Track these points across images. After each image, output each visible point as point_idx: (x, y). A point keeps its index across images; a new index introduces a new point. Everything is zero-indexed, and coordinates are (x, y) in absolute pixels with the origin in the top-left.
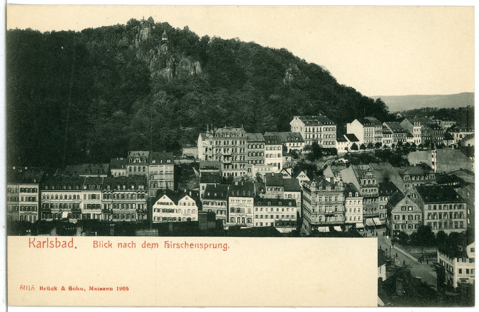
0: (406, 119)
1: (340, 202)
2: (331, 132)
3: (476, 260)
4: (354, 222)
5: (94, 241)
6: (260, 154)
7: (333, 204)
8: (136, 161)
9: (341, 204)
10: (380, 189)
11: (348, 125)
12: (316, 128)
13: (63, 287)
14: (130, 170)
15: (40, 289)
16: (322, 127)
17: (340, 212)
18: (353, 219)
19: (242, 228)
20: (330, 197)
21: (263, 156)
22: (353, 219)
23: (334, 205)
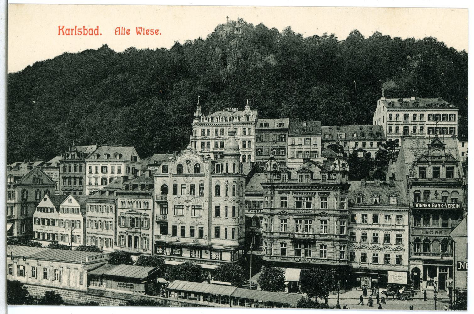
0: (71, 197)
2: (446, 123)
3: (380, 312)
4: (384, 268)
6: (279, 151)
7: (315, 215)
8: (72, 155)
11: (365, 38)
12: (411, 115)
14: (65, 171)
16: (426, 114)
17: (334, 238)
19: (230, 284)
21: (285, 155)
22: (369, 259)
23: (316, 218)
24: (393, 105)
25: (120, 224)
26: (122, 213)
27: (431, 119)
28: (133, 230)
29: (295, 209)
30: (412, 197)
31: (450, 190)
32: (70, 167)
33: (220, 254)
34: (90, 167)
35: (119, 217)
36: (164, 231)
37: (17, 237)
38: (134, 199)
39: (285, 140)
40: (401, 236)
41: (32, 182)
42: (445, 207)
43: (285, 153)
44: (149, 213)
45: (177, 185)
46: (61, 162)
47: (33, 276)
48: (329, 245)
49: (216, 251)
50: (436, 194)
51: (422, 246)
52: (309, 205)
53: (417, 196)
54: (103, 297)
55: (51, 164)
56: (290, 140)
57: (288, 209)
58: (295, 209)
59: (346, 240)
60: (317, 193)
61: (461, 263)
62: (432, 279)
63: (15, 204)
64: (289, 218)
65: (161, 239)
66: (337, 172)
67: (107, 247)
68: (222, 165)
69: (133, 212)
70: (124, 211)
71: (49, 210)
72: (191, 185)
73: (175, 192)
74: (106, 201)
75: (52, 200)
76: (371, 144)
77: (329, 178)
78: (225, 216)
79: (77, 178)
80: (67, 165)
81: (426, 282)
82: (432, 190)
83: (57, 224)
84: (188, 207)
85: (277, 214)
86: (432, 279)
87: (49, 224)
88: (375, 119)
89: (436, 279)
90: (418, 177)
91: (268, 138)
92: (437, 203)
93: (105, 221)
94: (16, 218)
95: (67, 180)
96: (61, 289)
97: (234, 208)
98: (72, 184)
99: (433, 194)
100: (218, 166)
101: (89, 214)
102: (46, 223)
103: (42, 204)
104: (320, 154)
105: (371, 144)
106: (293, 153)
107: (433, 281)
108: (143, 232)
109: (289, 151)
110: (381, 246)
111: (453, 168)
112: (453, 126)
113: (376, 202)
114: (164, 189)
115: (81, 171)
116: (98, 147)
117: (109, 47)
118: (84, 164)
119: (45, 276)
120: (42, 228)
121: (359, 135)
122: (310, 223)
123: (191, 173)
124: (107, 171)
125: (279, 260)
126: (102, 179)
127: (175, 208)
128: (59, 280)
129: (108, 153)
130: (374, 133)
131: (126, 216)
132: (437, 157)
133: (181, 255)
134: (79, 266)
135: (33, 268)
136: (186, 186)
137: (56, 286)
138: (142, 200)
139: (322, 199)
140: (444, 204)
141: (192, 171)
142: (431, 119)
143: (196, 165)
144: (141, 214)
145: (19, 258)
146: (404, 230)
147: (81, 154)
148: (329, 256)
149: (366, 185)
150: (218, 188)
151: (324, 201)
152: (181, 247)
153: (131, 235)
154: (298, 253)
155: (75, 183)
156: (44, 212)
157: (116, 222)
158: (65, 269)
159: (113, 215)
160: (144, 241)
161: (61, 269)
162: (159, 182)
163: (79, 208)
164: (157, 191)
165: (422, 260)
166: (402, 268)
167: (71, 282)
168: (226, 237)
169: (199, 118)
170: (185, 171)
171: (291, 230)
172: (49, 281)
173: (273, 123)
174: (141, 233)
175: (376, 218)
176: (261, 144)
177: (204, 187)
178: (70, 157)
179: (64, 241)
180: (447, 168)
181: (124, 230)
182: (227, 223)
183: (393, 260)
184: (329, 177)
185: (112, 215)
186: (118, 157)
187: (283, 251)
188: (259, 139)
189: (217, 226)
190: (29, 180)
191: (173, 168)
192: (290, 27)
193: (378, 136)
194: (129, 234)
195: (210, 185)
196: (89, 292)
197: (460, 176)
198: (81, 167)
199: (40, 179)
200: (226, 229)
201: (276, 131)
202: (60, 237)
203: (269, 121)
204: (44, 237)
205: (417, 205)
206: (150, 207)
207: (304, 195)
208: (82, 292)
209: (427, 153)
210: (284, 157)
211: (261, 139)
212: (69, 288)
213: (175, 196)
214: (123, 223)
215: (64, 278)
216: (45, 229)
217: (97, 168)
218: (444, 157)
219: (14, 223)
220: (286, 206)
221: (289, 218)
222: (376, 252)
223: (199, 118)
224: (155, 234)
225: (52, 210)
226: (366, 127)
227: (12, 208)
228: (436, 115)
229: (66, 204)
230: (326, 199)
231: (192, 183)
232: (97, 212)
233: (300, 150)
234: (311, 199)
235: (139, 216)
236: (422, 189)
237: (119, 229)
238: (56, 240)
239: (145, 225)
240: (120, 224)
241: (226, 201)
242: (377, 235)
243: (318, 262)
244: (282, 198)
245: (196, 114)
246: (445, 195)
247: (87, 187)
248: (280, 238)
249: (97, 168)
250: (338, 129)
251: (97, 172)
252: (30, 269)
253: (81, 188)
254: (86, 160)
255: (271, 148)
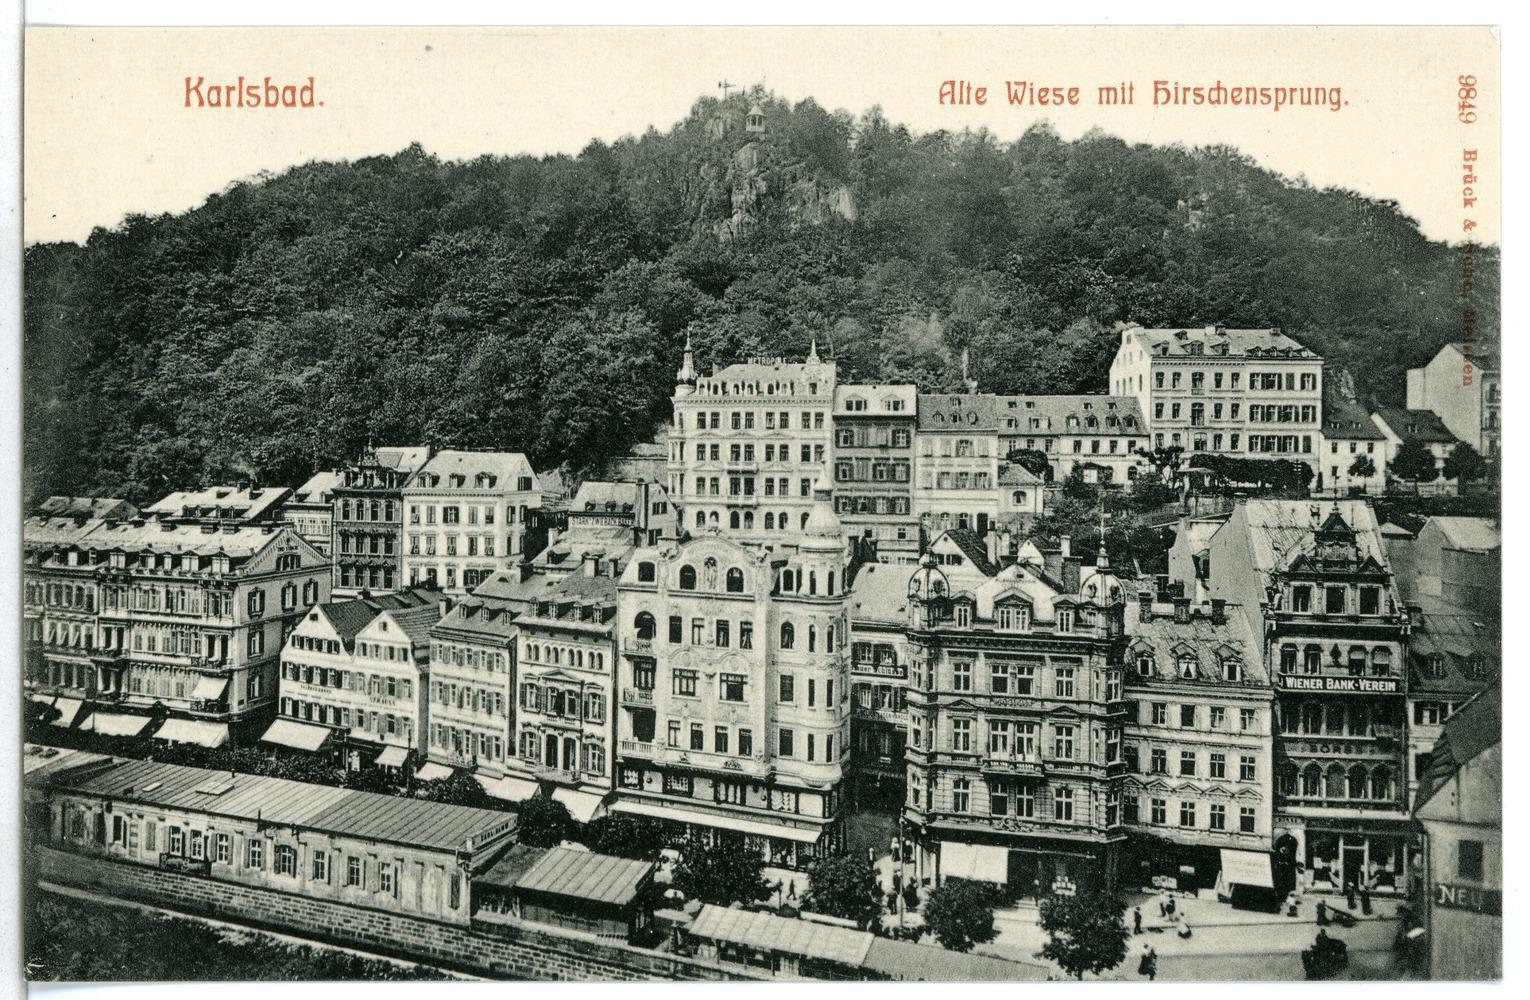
0: (385, 616)
1: (1084, 708)
5: (1156, 83)
7: (1042, 714)
8: (365, 476)
9: (1092, 717)
10: (930, 851)
13: (1473, 224)
14: (346, 515)
15: (1466, 153)
18: (1203, 819)
19: (854, 923)
20: (1021, 671)
22: (1203, 819)
24: (1165, 350)
25: (523, 702)
26: (529, 676)
27: (1258, 384)
28: (560, 722)
29: (991, 698)
30: (1277, 660)
31: (1370, 645)
32: (360, 506)
33: (793, 796)
34: (413, 510)
35: (522, 685)
36: (644, 722)
37: (239, 716)
38: (564, 644)
39: (908, 442)
40: (1252, 760)
41: (274, 567)
42: (1358, 688)
43: (908, 475)
44: (606, 683)
45: (679, 619)
46: (337, 494)
47: (318, 874)
48: (1080, 792)
49: (784, 789)
50: (1336, 653)
51: (1301, 781)
52: (1025, 686)
53: (1288, 658)
54: (515, 944)
55: (306, 496)
56: (919, 443)
57: (975, 696)
58: (991, 698)
59: (1119, 776)
60: (1048, 660)
61: (1444, 889)
62: (1326, 865)
63: (233, 629)
64: (975, 720)
65: (638, 752)
66: (1099, 609)
67: (489, 758)
68: (799, 573)
69: (559, 677)
70: (537, 671)
71: (325, 646)
72: (718, 622)
73: (675, 635)
74: (489, 640)
75: (331, 620)
76: (1113, 445)
77: (1078, 622)
78: (807, 702)
79: (380, 535)
80: (353, 502)
81: (1311, 872)
82: (1327, 643)
83: (345, 682)
84: (711, 677)
85: (947, 707)
86: (1326, 865)
87: (324, 682)
88: (1116, 373)
89: (1338, 865)
90: (1291, 611)
91: (865, 438)
92: (1340, 679)
93: (483, 692)
94: (236, 666)
95: (353, 541)
96: (399, 915)
97: (830, 683)
98: (367, 550)
99: (1327, 653)
100: (788, 574)
101: (436, 667)
102: (317, 679)
103: (305, 628)
104: (995, 481)
105: (1113, 445)
106: (930, 475)
107: (1329, 869)
108: (588, 729)
109: (919, 467)
110: (1205, 786)
111: (1376, 591)
112: (1312, 403)
113: (1188, 673)
114: (645, 625)
115: (389, 516)
116: (432, 455)
117: (429, 151)
118: (397, 504)
119: (353, 880)
120: (306, 691)
121: (1083, 421)
122: (1030, 731)
123: (718, 590)
124: (457, 520)
125: (949, 824)
126: (466, 573)
127: (675, 676)
128: (392, 892)
129: (459, 472)
130: (1120, 417)
131: (541, 683)
132: (1336, 563)
133: (689, 794)
134: (450, 861)
135: (320, 854)
136: (706, 623)
137: (384, 907)
138: (586, 648)
139: (1060, 672)
140: (1357, 681)
141: (721, 587)
142: (1258, 384)
143: (731, 571)
144: (582, 683)
145: (280, 826)
146: (1261, 748)
147: (391, 475)
148: (1080, 815)
149: (1154, 617)
150: (788, 631)
151: (1065, 679)
152: (689, 774)
153: (556, 733)
154: (998, 806)
155: (374, 548)
156: (311, 648)
157: (512, 696)
158: (409, 862)
159: (505, 680)
160: (591, 751)
161: (399, 863)
162: (629, 608)
163: (409, 647)
164: (626, 628)
165: (1302, 818)
166: (1256, 843)
167: (427, 899)
168: (811, 757)
169: (691, 382)
170: (701, 586)
171: (981, 749)
172: (364, 893)
173: (875, 398)
174: (581, 731)
175: (1188, 715)
176: (847, 453)
177: (754, 627)
178: (360, 482)
179: (368, 730)
180: (1362, 589)
181: (538, 720)
182: (814, 721)
183: (1233, 821)
184: (1078, 619)
185: (501, 678)
186: (486, 482)
187: (961, 800)
188: (844, 438)
189: (787, 727)
190: (268, 564)
191: (668, 575)
192: (877, 109)
193: (1130, 425)
194: (550, 732)
195: (770, 621)
196: (476, 928)
197: (1392, 610)
198: (389, 506)
199: (293, 556)
200: (811, 737)
201: (880, 421)
202: (354, 717)
203: (864, 391)
204: (309, 716)
205: (1290, 682)
206: (608, 666)
207: (1013, 663)
208: (457, 926)
209: (1312, 553)
210: (905, 486)
211: (848, 440)
212: (419, 915)
213: (676, 646)
214: (531, 699)
215: (408, 886)
216: (313, 693)
217: (431, 511)
218: (1353, 563)
219: (231, 679)
220: (967, 687)
221: (975, 720)
222: (1191, 797)
223: (691, 382)
224: (620, 738)
225: (333, 647)
226: (1097, 401)
227: (225, 641)
228: (1269, 375)
229: (371, 633)
230: (1070, 673)
231: (723, 617)
232: (461, 664)
233: (945, 469)
234: (1030, 672)
235: (576, 689)
236: (1301, 641)
237: (522, 717)
238: (344, 724)
239: (594, 710)
240: (523, 702)
241: (808, 665)
242: (1192, 755)
243: (1052, 834)
244: (957, 668)
245: (686, 372)
246: (1357, 656)
247: (406, 560)
248: (952, 768)
249: (431, 511)
250: (1029, 405)
251: (431, 521)
252: (311, 858)
253: (390, 562)
254: (404, 491)
255: (873, 461)
